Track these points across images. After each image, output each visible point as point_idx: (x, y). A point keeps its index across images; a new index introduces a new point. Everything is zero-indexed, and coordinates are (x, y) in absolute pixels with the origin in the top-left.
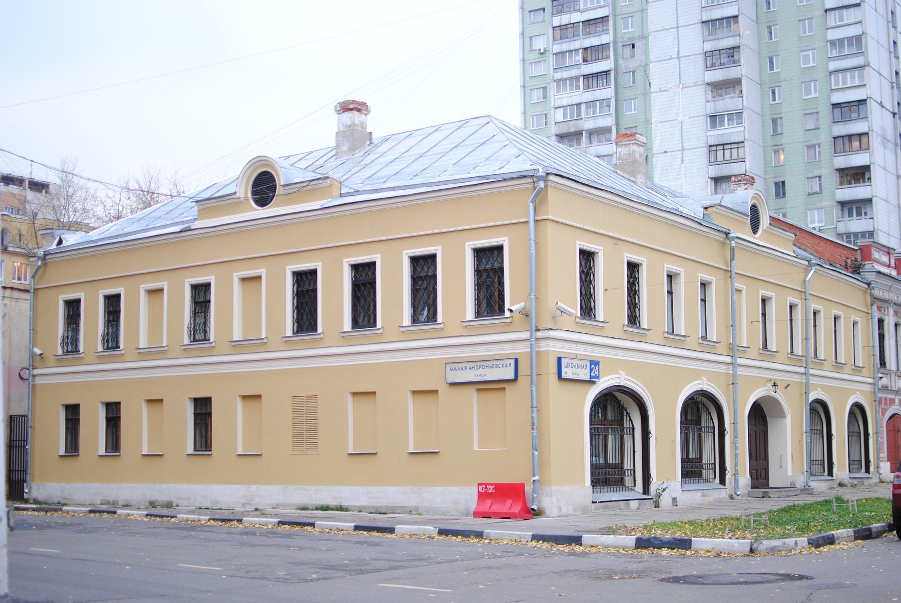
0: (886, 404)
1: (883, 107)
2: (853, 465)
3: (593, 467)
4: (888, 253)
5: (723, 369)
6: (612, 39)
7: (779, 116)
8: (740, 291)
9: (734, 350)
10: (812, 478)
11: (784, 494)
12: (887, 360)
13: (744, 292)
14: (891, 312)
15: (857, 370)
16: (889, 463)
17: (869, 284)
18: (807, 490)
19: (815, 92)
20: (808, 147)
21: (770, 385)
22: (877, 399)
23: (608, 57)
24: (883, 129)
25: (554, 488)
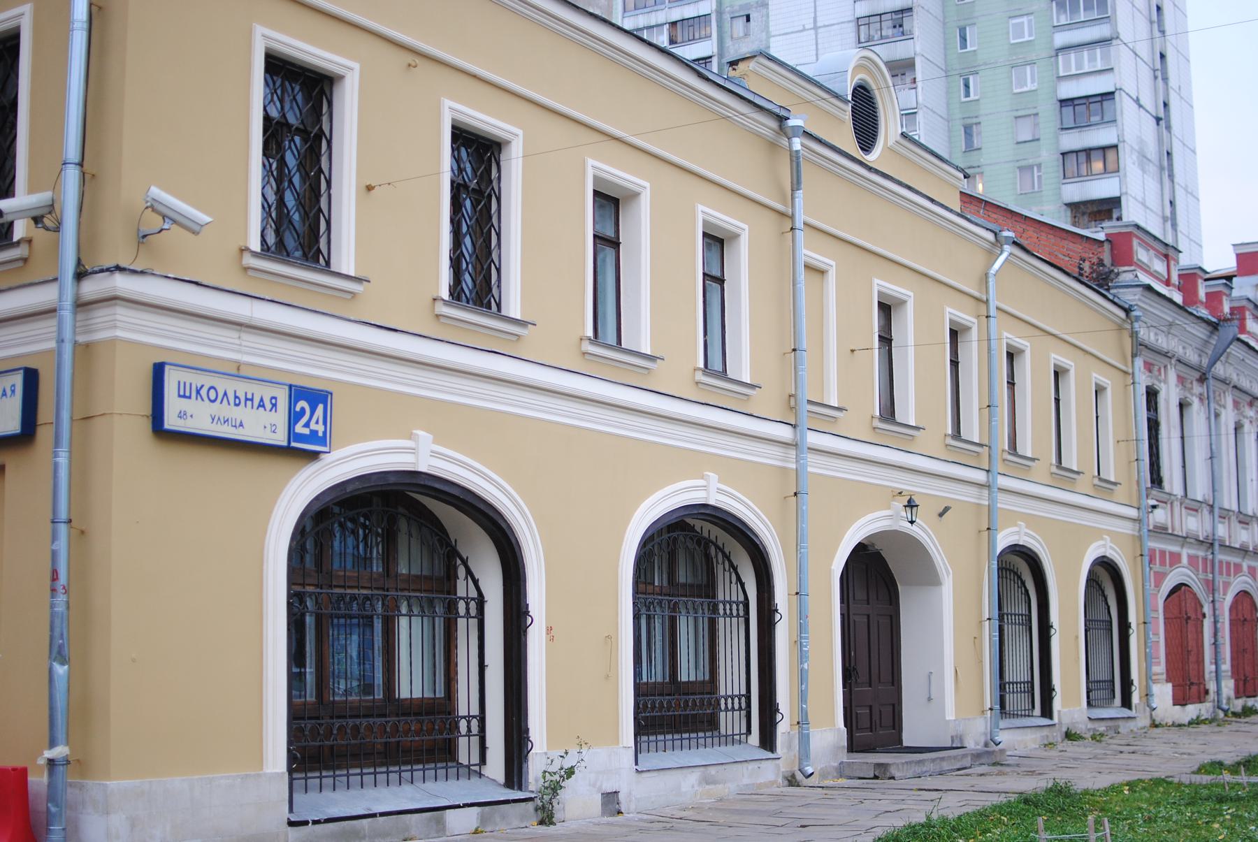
0: (1163, 563)
1: (1140, 106)
2: (1097, 692)
3: (641, 691)
4: (1166, 256)
5: (769, 456)
6: (714, 7)
7: (975, 121)
8: (822, 272)
9: (796, 411)
10: (1003, 724)
11: (930, 767)
12: (1165, 473)
14: (1172, 376)
15: (1105, 487)
16: (1170, 685)
17: (1127, 311)
18: (990, 756)
19: (1033, 82)
20: (1021, 168)
21: (900, 504)
22: (1146, 552)
23: (709, 37)
24: (1141, 141)
25: (112, 784)
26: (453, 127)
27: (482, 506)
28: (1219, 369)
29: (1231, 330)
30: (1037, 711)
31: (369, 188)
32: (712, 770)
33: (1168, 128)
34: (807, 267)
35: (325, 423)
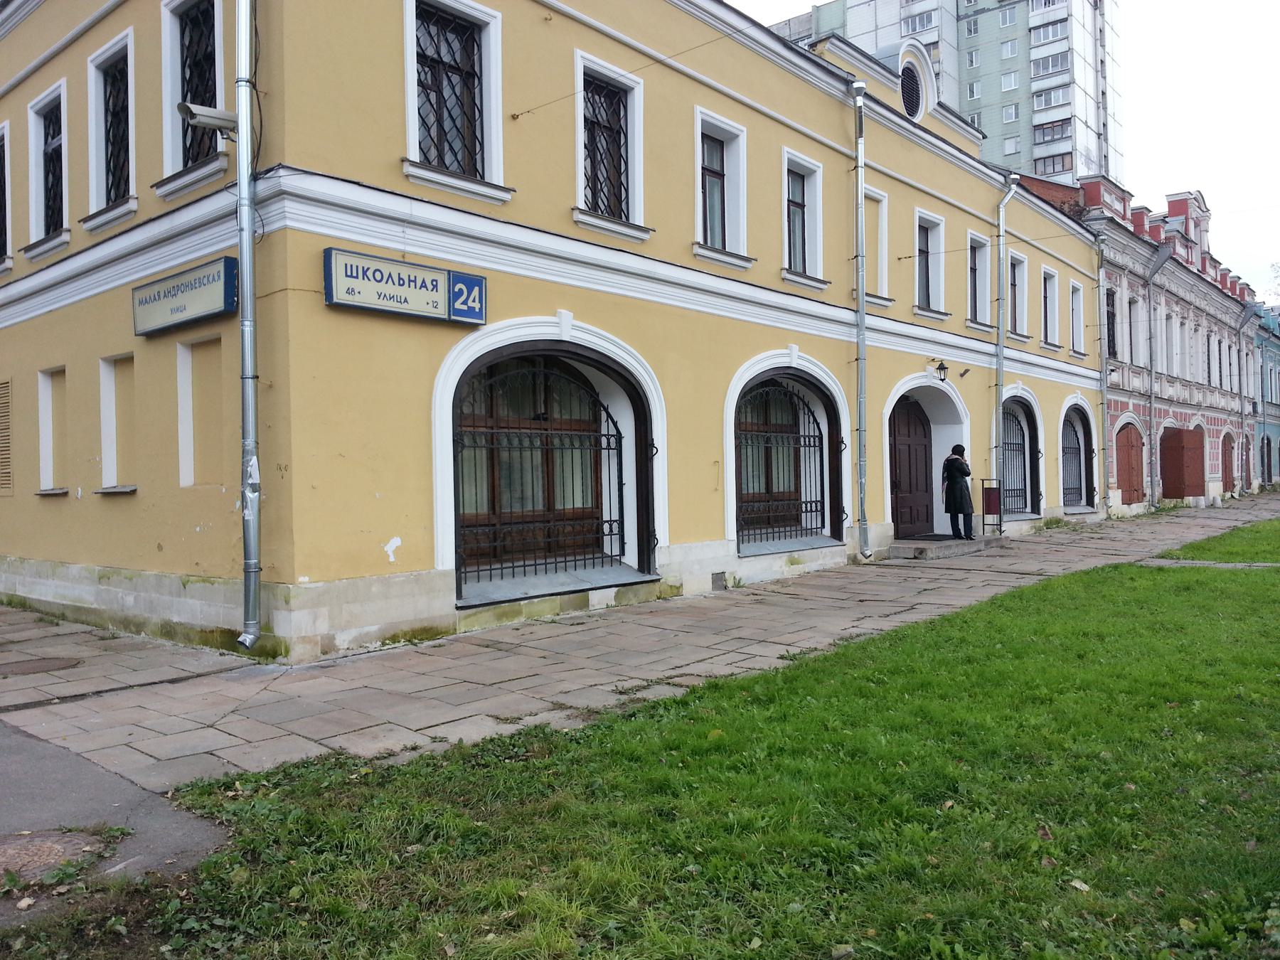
0: (1116, 410)
2: (1071, 495)
8: (877, 201)
12: (1119, 348)
13: (885, 203)
14: (1125, 282)
21: (932, 368)
24: (1088, 150)
26: (585, 74)
27: (615, 367)
28: (1158, 279)
29: (1166, 252)
30: (1029, 509)
31: (514, 117)
32: (796, 555)
33: (1106, 140)
34: (867, 197)
35: (481, 302)
